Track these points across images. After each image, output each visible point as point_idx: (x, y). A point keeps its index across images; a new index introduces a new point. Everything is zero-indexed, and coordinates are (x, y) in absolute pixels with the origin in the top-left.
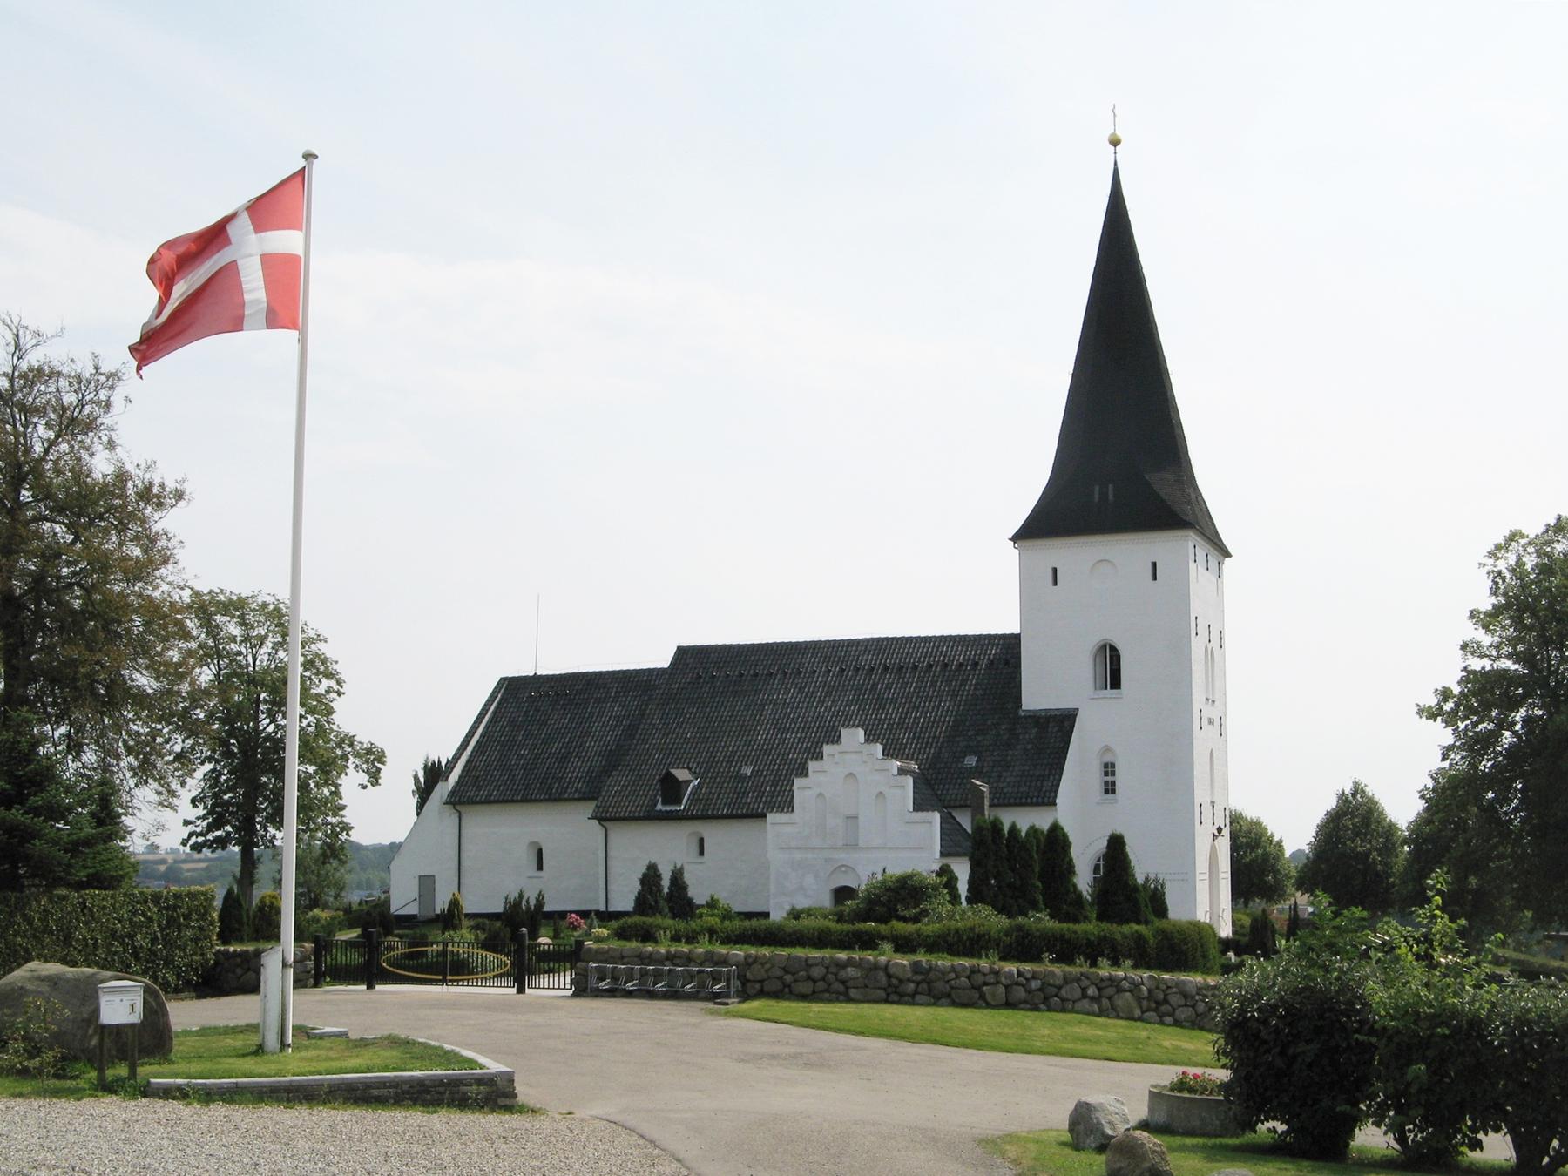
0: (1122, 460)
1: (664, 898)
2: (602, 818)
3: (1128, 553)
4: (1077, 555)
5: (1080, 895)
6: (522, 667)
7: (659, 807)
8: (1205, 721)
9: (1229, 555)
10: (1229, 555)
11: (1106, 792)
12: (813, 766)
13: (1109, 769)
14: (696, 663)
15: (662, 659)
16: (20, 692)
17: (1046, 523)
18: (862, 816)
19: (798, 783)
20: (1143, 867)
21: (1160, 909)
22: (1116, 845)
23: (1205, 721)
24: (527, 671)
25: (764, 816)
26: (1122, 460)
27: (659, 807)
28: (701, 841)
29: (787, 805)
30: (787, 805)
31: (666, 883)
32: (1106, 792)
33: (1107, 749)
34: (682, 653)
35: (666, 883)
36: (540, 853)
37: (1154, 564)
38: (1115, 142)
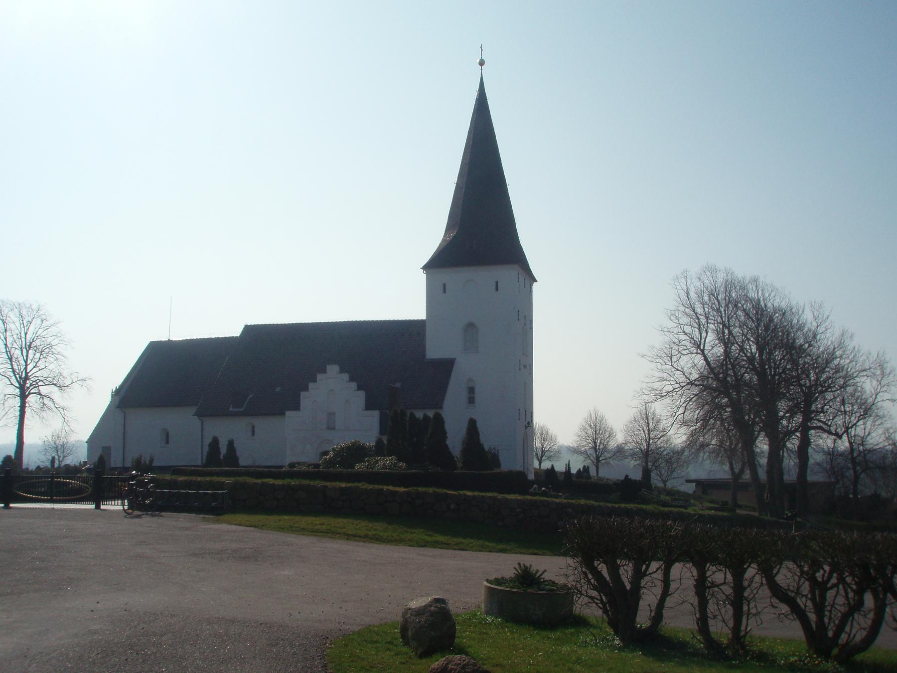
0: (481, 232)
1: (220, 458)
2: (200, 415)
3: (484, 276)
4: (456, 277)
5: (451, 457)
6: (162, 336)
7: (231, 409)
8: (522, 367)
9: (536, 281)
10: (536, 281)
11: (470, 402)
12: (311, 385)
13: (471, 390)
14: (256, 336)
15: (235, 331)
16: (885, 534)
17: (439, 263)
18: (336, 416)
19: (303, 394)
20: (488, 440)
21: (497, 464)
22: (472, 424)
23: (522, 367)
24: (164, 338)
25: (284, 414)
26: (481, 232)
27: (231, 409)
28: (253, 427)
29: (296, 407)
30: (296, 407)
31: (223, 450)
32: (470, 402)
33: (470, 380)
34: (248, 329)
35: (223, 450)
36: (167, 435)
37: (497, 283)
38: (482, 63)
